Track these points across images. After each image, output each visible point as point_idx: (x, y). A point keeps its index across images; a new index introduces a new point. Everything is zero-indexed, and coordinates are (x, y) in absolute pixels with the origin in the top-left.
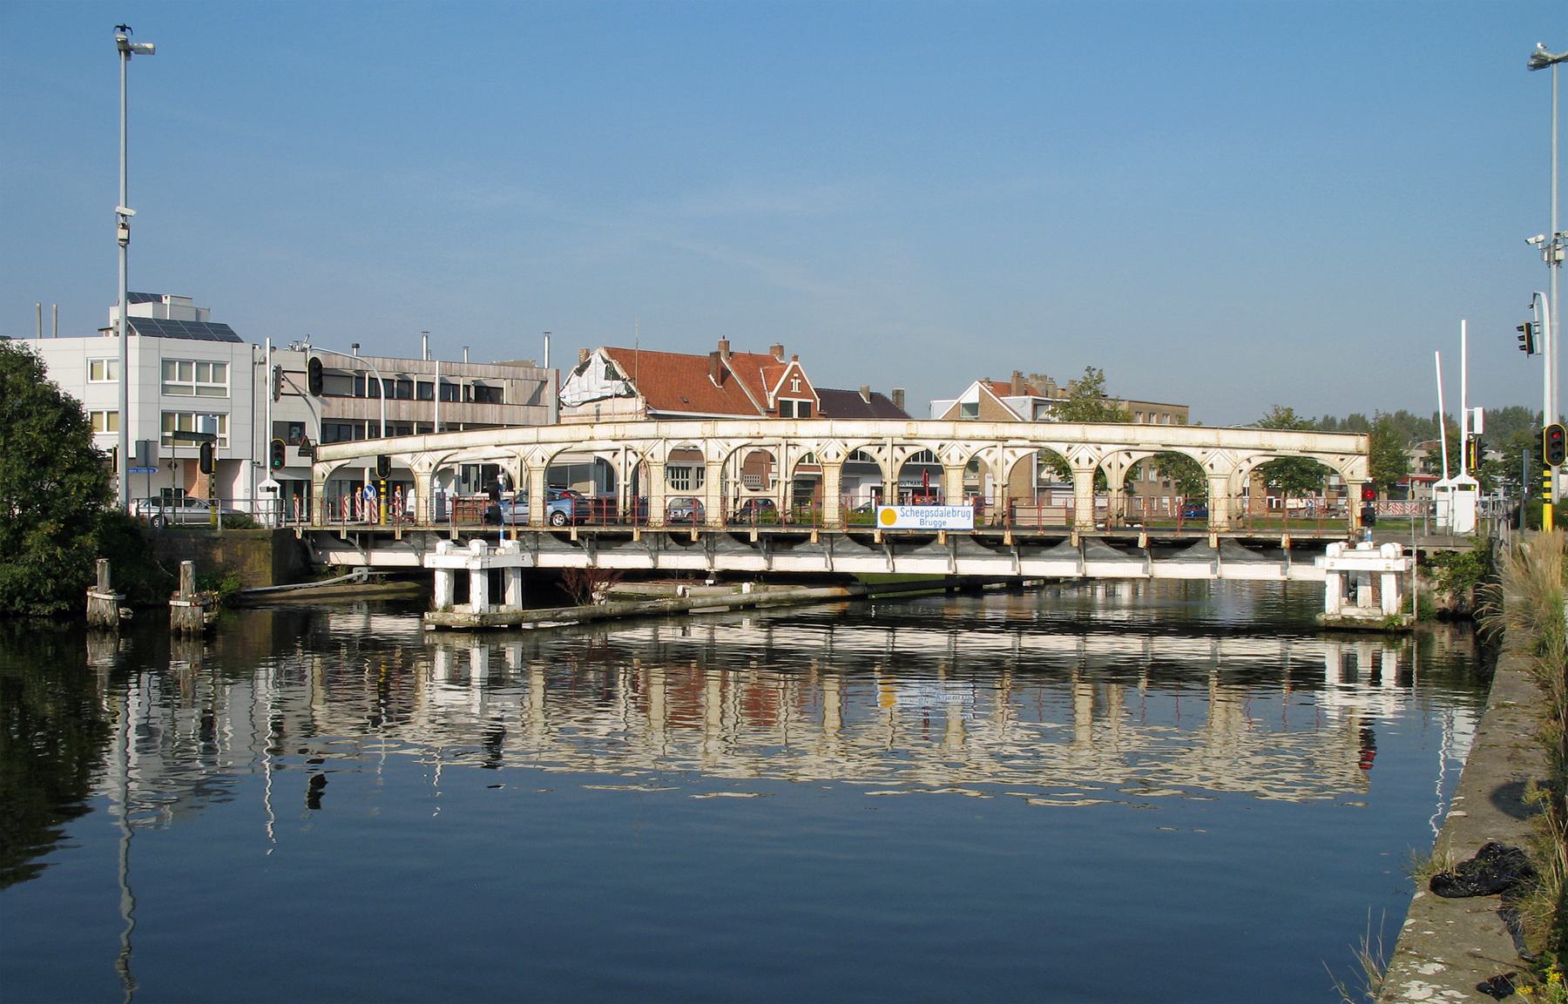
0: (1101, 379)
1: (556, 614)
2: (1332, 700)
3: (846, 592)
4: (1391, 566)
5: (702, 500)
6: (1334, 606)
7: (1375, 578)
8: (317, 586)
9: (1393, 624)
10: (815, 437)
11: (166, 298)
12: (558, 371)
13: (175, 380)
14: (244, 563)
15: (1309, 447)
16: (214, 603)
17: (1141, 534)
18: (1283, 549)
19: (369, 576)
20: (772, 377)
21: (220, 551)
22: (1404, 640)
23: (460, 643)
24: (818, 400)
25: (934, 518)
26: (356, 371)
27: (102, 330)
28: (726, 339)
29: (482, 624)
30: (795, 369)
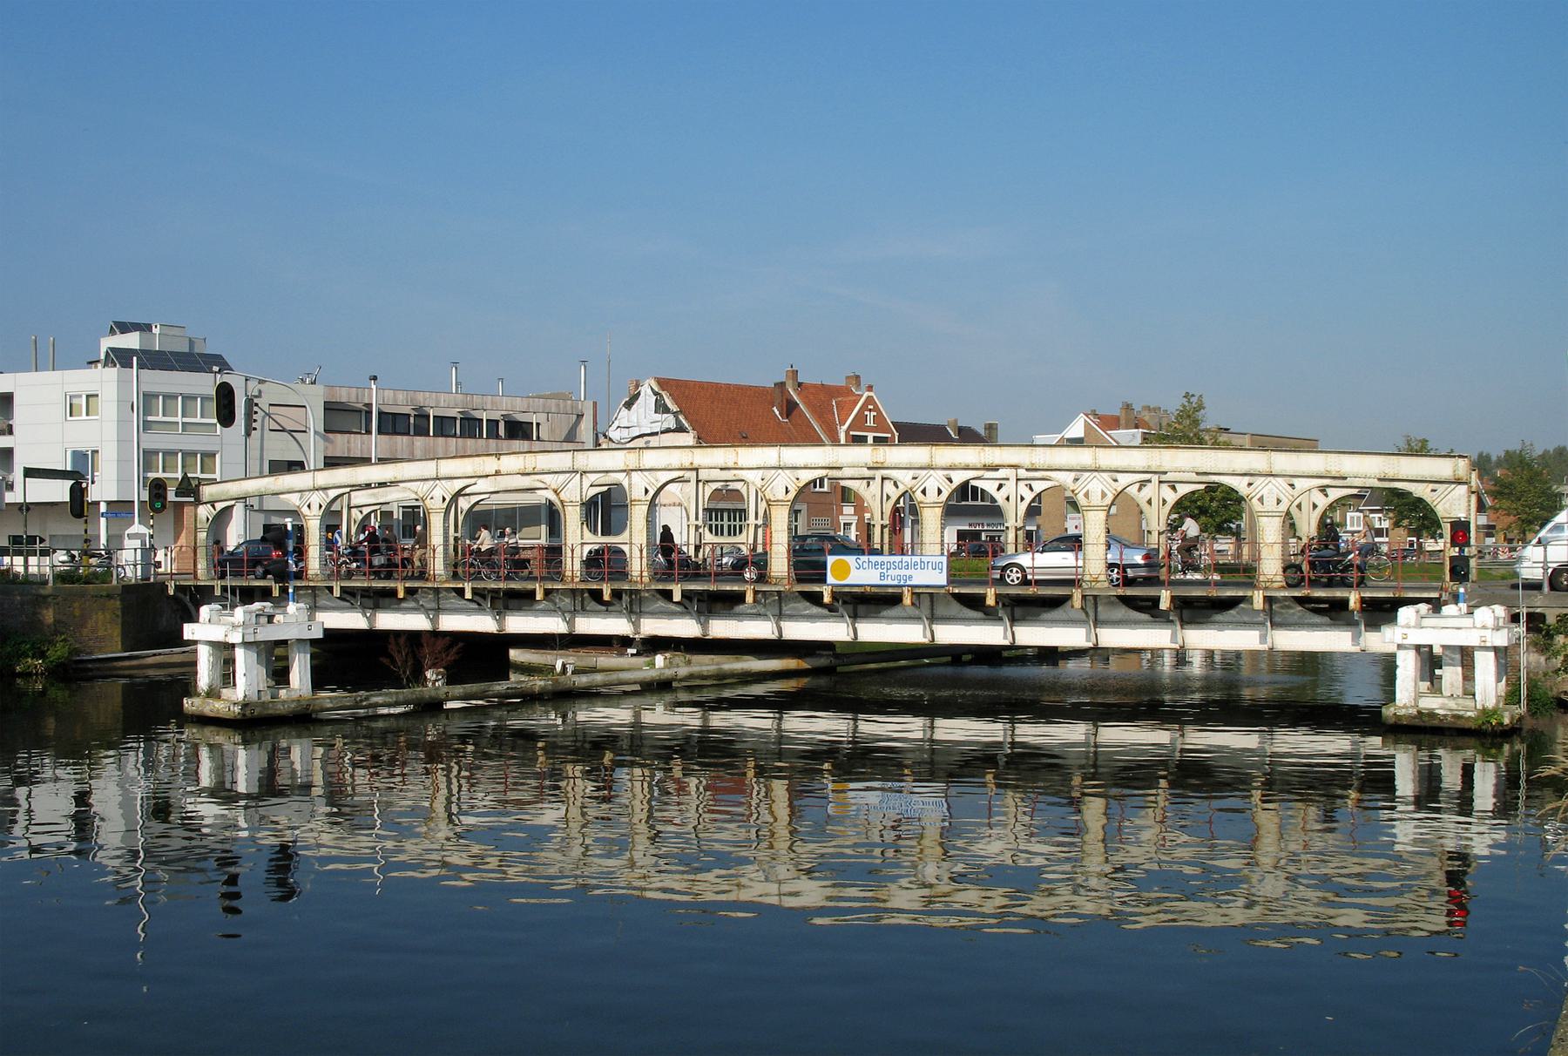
0: (1200, 407)
1: (361, 701)
2: (1406, 831)
3: (803, 664)
4: (1489, 639)
5: (626, 548)
6: (1408, 694)
7: (1466, 656)
8: (184, 652)
9: (1489, 722)
11: (156, 327)
12: (595, 404)
13: (158, 416)
14: (83, 625)
16: (37, 674)
17: (1163, 591)
18: (1353, 611)
20: (845, 410)
21: (51, 610)
22: (1506, 747)
23: (220, 738)
24: (896, 434)
25: (897, 572)
27: (91, 363)
29: (244, 715)
30: (870, 400)
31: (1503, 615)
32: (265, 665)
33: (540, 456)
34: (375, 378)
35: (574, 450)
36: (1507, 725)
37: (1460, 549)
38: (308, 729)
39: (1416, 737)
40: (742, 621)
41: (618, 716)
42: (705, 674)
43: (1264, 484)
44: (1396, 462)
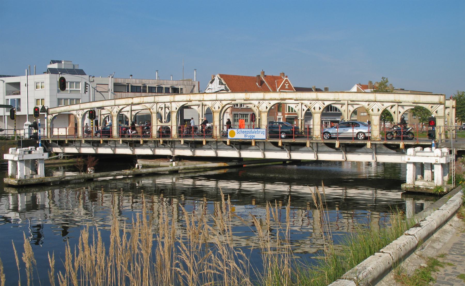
3: (227, 165)
4: (438, 161)
7: (432, 166)
10: (210, 101)
12: (199, 82)
15: (354, 99)
17: (337, 141)
19: (63, 156)
20: (279, 83)
26: (127, 84)
28: (263, 71)
29: (19, 184)
30: (286, 80)
31: (447, 152)
32: (30, 167)
33: (145, 98)
34: (132, 76)
35: (155, 96)
36: (445, 192)
37: (433, 127)
38: (42, 188)
39: (414, 196)
40: (205, 150)
41: (167, 181)
42: (190, 168)
43: (373, 105)
44: (419, 97)
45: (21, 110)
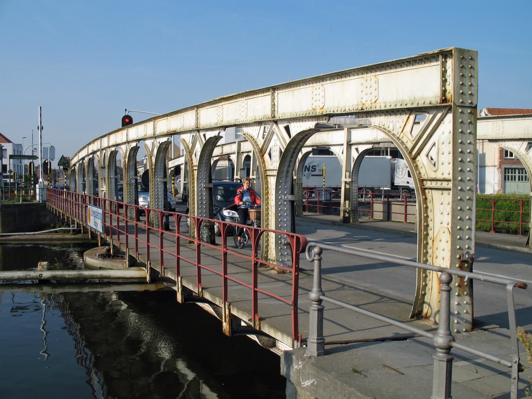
45: (284, 128)
